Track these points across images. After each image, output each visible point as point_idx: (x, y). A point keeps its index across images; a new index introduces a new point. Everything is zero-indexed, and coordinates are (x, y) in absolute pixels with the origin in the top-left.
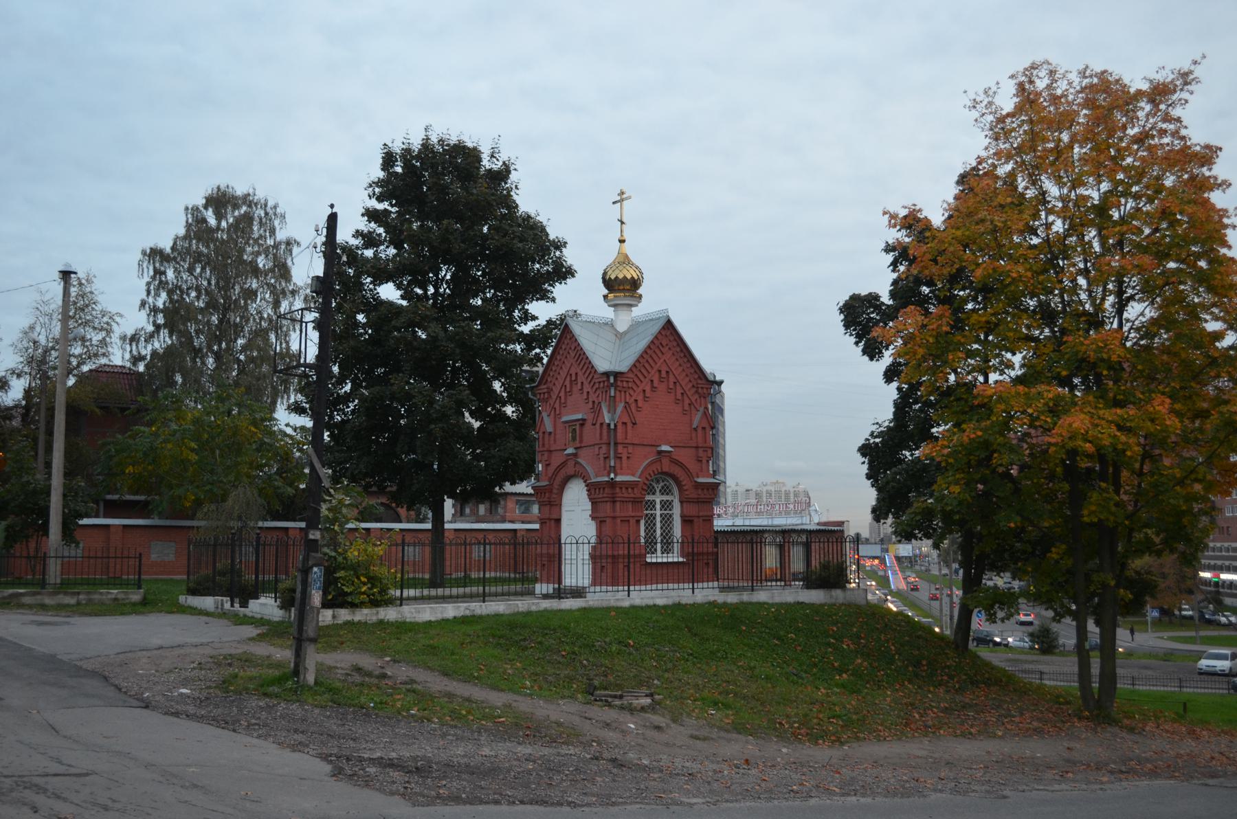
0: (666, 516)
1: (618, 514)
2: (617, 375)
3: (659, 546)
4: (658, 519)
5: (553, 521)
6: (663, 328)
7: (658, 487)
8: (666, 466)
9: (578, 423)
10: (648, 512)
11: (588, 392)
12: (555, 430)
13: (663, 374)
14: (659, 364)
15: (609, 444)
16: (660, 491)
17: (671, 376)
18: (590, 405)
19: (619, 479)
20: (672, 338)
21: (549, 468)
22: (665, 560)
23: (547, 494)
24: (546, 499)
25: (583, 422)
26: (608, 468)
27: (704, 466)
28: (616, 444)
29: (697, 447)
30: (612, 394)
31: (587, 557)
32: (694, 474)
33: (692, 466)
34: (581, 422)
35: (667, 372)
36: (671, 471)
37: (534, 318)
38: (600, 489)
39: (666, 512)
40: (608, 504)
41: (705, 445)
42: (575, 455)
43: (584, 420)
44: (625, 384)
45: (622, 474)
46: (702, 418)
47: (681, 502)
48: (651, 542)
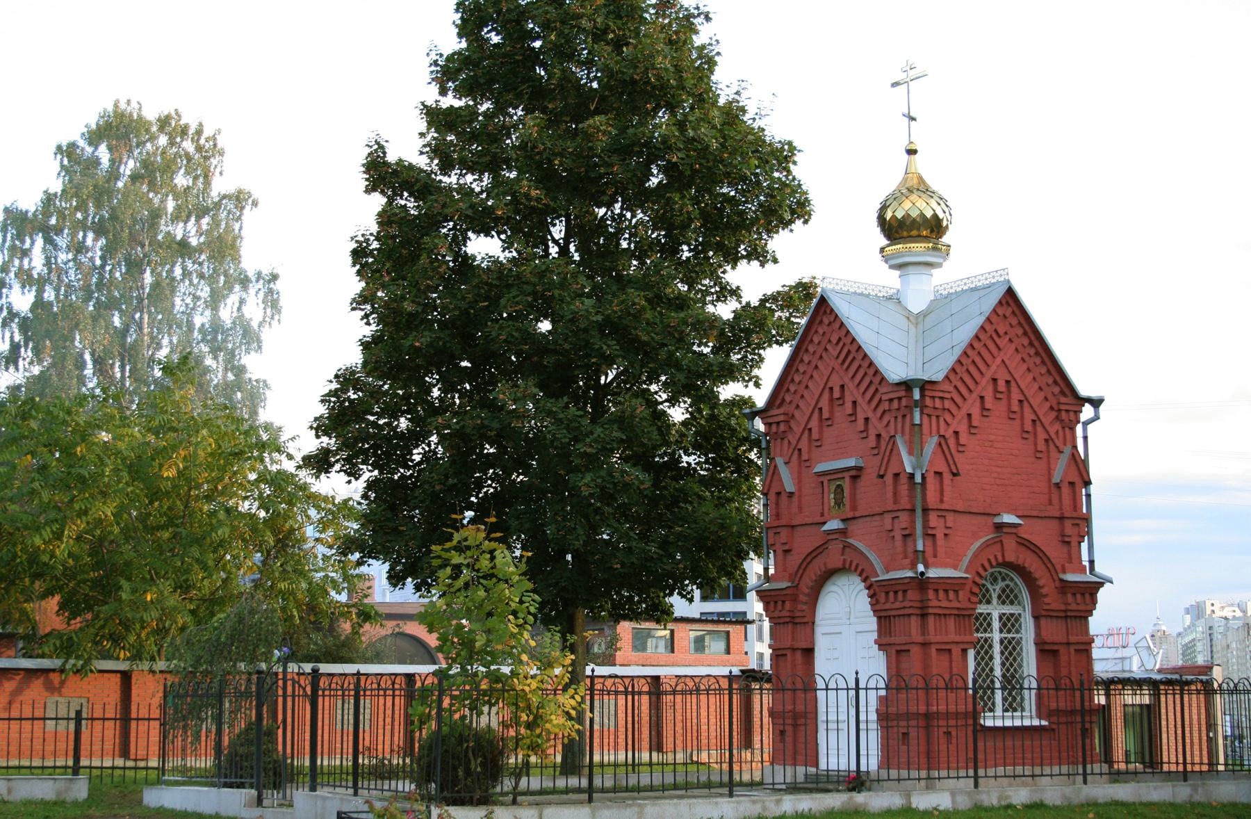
0: (1010, 642)
1: (932, 638)
2: (925, 385)
3: (998, 696)
4: (997, 648)
5: (799, 654)
6: (1000, 302)
7: (995, 590)
8: (1012, 553)
9: (847, 475)
10: (979, 635)
11: (867, 419)
12: (800, 490)
13: (1002, 386)
14: (993, 368)
15: (913, 510)
16: (999, 597)
17: (1014, 389)
18: (872, 442)
19: (933, 573)
20: (1014, 321)
21: (789, 557)
22: (1008, 723)
23: (788, 604)
24: (784, 613)
25: (856, 474)
26: (911, 555)
27: (1074, 552)
28: (925, 510)
29: (1061, 518)
30: (917, 420)
31: (873, 716)
32: (1058, 567)
33: (1054, 552)
34: (853, 473)
35: (1008, 382)
36: (1020, 562)
37: (735, 293)
38: (896, 593)
39: (1010, 636)
40: (913, 619)
41: (1075, 515)
42: (843, 532)
43: (859, 469)
44: (938, 403)
45: (937, 565)
46: (1068, 465)
47: (1036, 618)
48: (984, 688)
